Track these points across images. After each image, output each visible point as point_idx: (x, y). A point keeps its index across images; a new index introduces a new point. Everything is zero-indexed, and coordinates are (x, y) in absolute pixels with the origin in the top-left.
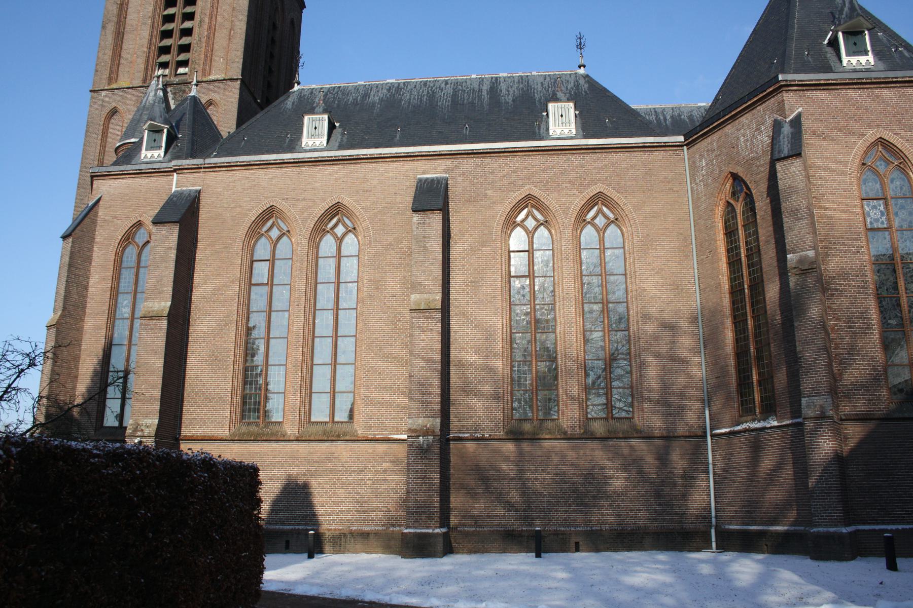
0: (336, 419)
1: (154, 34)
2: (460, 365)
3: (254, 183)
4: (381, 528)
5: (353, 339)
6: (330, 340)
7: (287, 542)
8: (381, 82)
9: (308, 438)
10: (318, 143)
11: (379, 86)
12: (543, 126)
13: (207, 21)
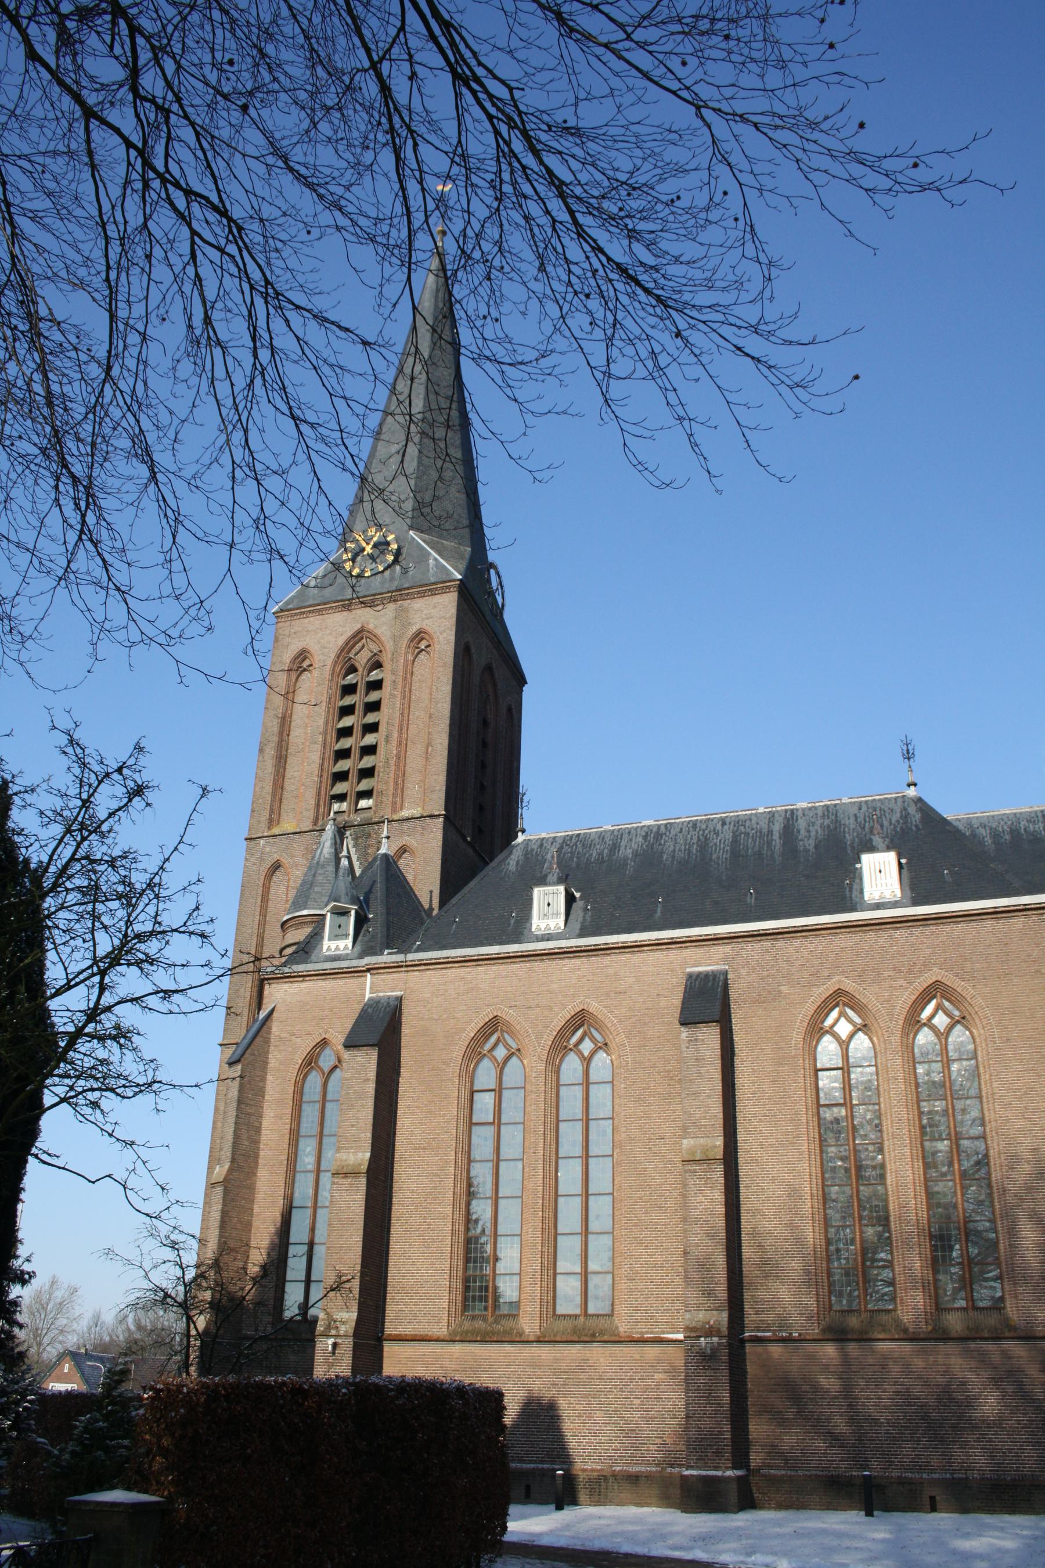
0: (591, 1310)
1: (327, 756)
2: (754, 1234)
3: (470, 985)
4: (654, 1469)
5: (609, 1198)
6: (578, 1200)
7: (528, 1488)
8: (635, 825)
9: (553, 1338)
10: (552, 925)
11: (633, 831)
12: (855, 886)
13: (395, 735)
